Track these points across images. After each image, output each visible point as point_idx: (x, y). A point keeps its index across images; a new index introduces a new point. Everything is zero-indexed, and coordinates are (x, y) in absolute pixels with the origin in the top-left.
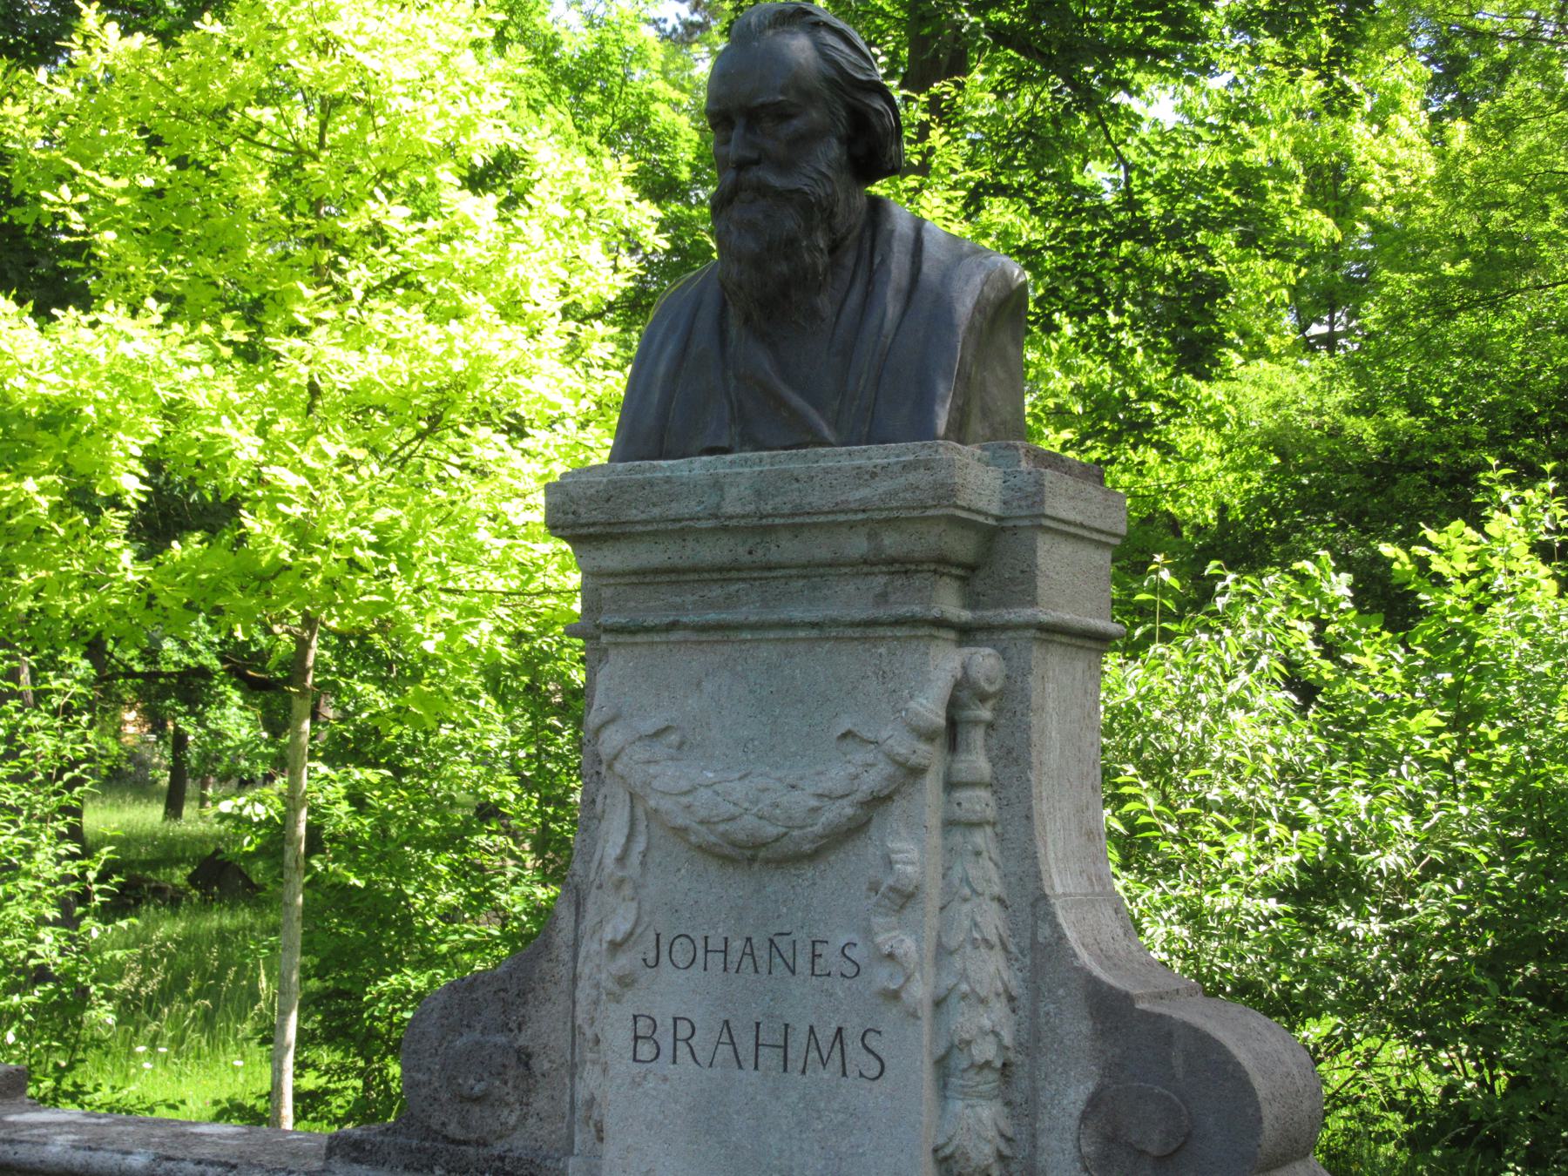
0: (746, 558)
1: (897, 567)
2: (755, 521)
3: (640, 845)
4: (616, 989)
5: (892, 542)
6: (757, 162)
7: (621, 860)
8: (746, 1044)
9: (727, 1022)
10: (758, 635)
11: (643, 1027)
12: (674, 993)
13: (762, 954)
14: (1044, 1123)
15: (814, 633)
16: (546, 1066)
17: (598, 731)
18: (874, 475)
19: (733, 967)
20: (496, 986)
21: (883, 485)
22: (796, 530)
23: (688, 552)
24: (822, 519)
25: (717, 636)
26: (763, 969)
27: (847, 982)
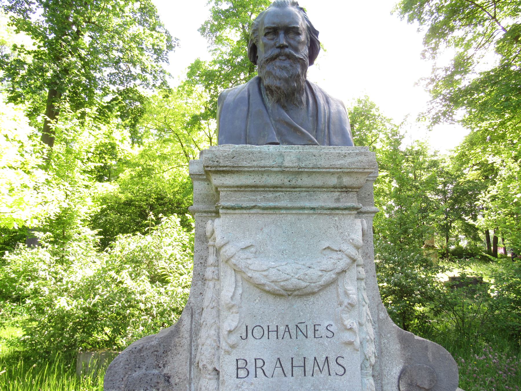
0: (287, 183)
1: (344, 189)
2: (297, 169)
3: (240, 291)
4: (230, 349)
5: (347, 181)
6: (287, 47)
8: (287, 367)
9: (279, 359)
10: (288, 212)
11: (241, 364)
12: (254, 349)
13: (293, 331)
14: (385, 381)
15: (312, 212)
16: (177, 380)
18: (345, 156)
19: (280, 337)
20: (152, 350)
21: (349, 160)
22: (310, 174)
23: (263, 180)
24: (324, 170)
25: (271, 212)
26: (294, 337)
27: (329, 339)
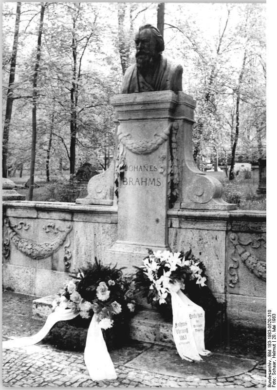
7: (122, 155)
8: (140, 182)
13: (143, 168)
17: (118, 136)
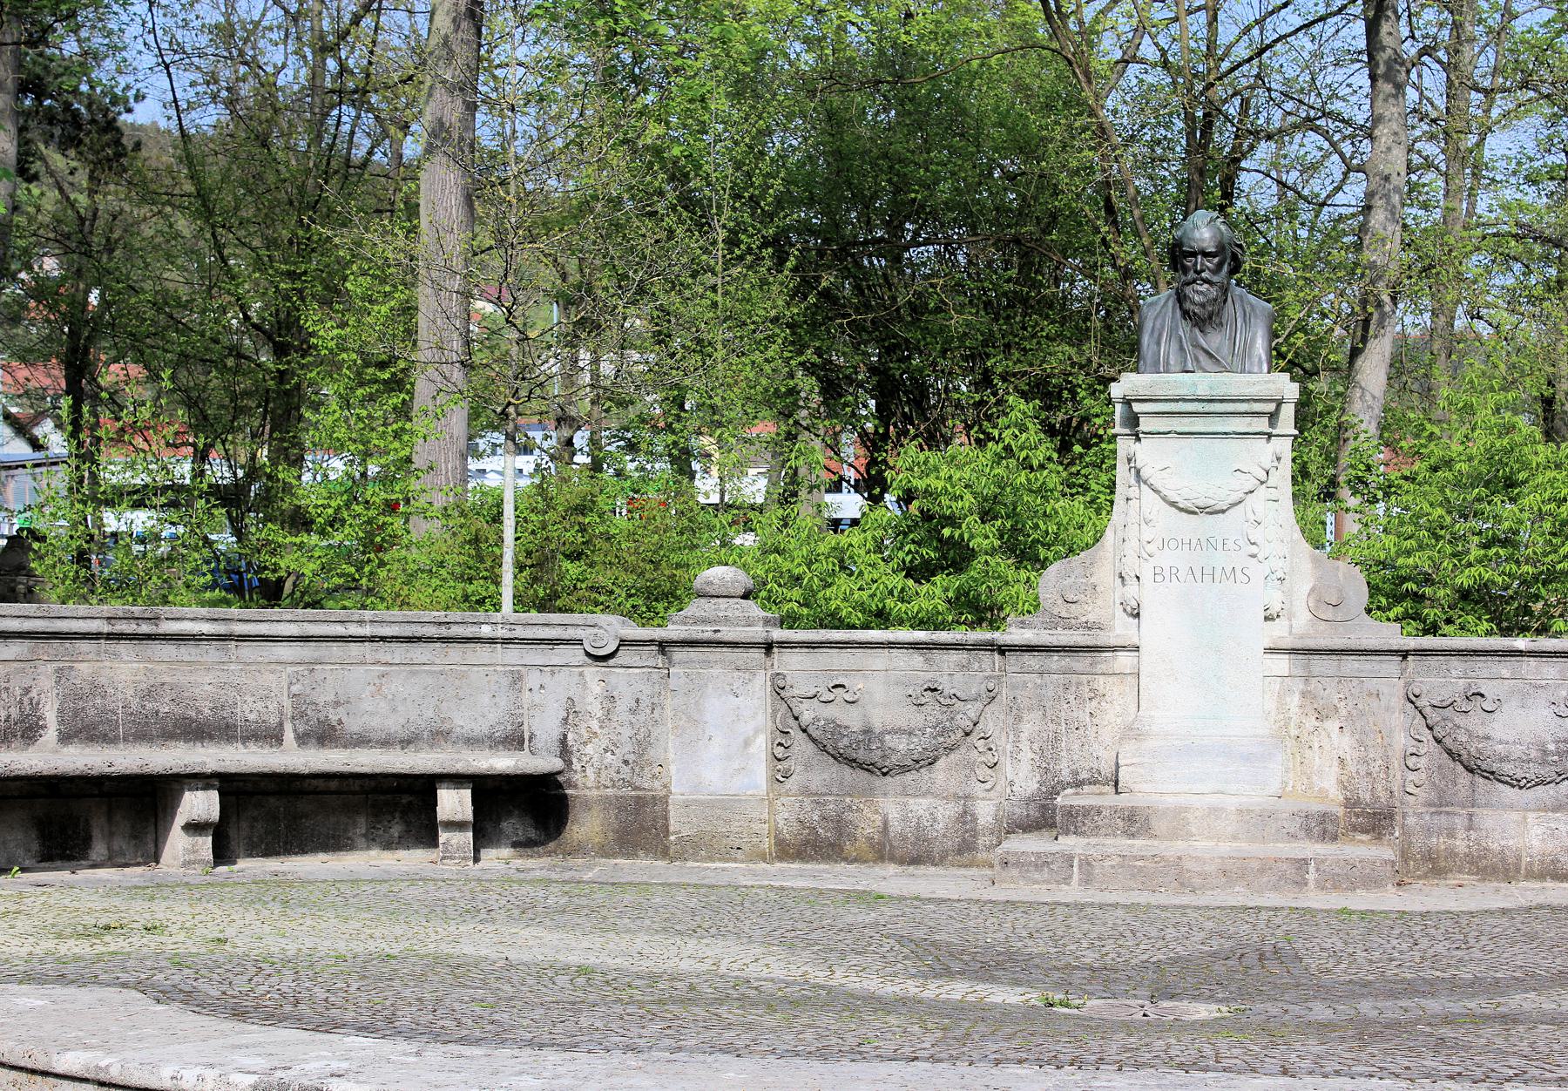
8: (1198, 575)
13: (1204, 543)
